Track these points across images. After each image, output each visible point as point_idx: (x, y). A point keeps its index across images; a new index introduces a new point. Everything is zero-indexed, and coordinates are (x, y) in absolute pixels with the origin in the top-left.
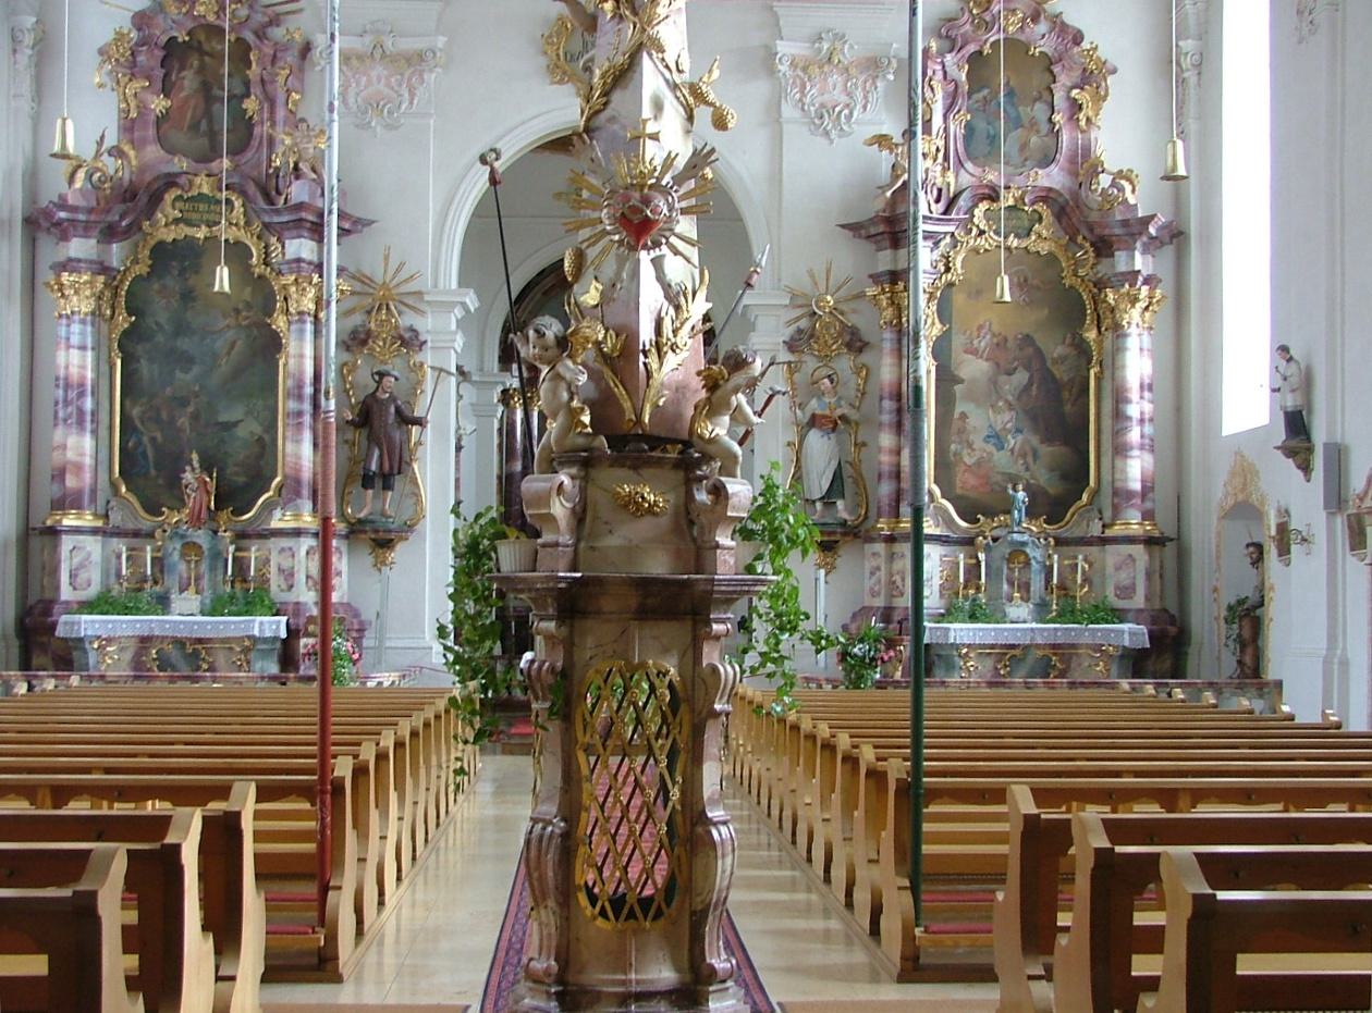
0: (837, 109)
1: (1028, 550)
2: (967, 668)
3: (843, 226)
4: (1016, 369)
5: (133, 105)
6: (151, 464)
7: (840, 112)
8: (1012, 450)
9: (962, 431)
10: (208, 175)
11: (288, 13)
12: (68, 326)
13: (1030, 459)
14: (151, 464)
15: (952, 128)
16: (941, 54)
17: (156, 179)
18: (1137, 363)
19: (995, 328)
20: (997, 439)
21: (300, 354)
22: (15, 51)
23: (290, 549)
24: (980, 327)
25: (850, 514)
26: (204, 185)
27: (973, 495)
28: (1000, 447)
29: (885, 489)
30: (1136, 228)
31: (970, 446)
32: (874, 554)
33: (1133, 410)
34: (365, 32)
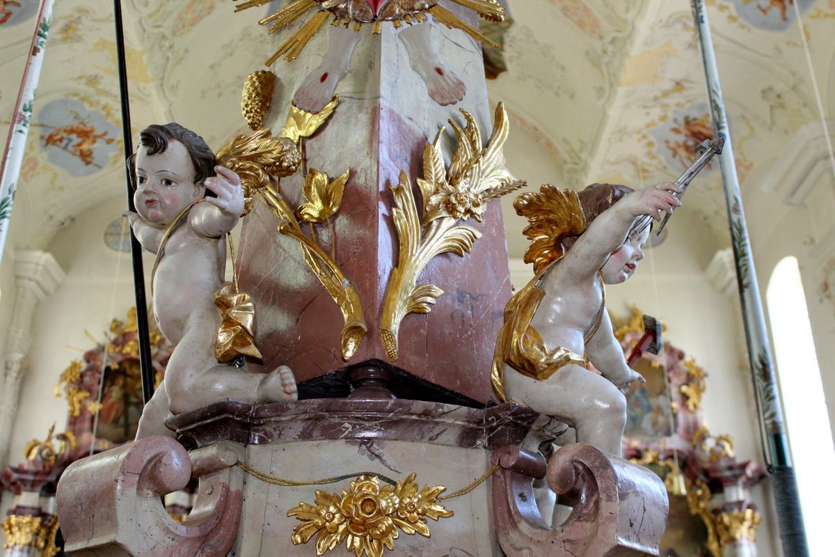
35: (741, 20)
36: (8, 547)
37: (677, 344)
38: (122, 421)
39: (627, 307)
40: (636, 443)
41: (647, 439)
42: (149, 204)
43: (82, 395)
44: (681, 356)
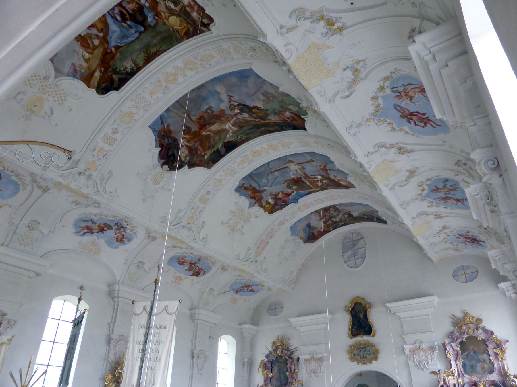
0: (424, 362)
7: (425, 363)
37: (489, 327)
38: (279, 379)
39: (462, 311)
41: (480, 376)
42: (409, 58)
43: (267, 371)
44: (492, 333)
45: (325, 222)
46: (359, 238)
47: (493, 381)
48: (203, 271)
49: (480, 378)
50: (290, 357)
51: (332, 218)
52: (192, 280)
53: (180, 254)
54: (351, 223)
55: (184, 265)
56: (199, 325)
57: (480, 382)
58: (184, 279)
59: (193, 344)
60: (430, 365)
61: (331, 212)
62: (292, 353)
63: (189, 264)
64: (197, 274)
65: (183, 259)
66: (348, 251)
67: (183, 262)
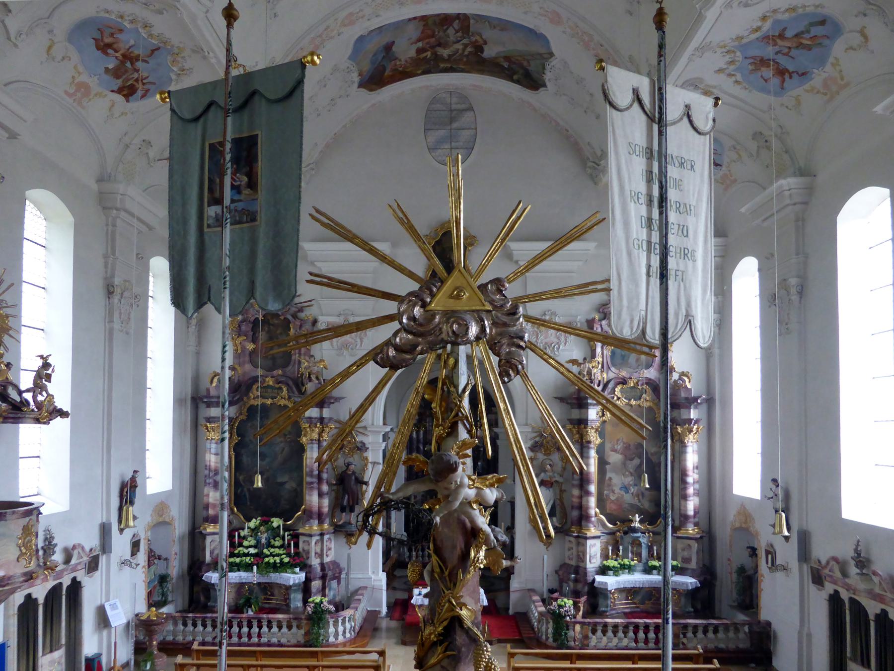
0: (553, 345)
1: (640, 539)
2: (614, 598)
3: (556, 398)
4: (634, 458)
5: (239, 348)
6: (248, 500)
7: (554, 346)
8: (632, 494)
9: (609, 485)
10: (272, 377)
11: (306, 306)
12: (210, 443)
13: (641, 497)
14: (248, 500)
15: (605, 352)
16: (600, 320)
17: (250, 379)
18: (692, 458)
19: (625, 440)
20: (626, 489)
21: (311, 455)
22: (188, 327)
23: (308, 542)
24: (618, 440)
25: (560, 524)
26: (270, 382)
27: (615, 513)
28: (627, 492)
29: (575, 513)
30: (692, 401)
31: (613, 492)
32: (570, 541)
33: (690, 480)
34: (341, 314)
35: (744, 85)
36: (207, 439)
40: (624, 374)
41: (631, 370)
43: (241, 339)
45: (419, 51)
46: (463, 106)
47: (650, 379)
48: (146, 87)
49: (632, 374)
50: (295, 316)
51: (439, 45)
52: (113, 106)
53: (113, 17)
54: (462, 71)
55: (106, 54)
56: (119, 222)
57: (631, 378)
58: (96, 95)
59: (110, 266)
60: (563, 350)
61: (451, 31)
62: (301, 310)
63: (121, 58)
64: (128, 92)
65: (112, 35)
66: (437, 130)
67: (109, 46)
